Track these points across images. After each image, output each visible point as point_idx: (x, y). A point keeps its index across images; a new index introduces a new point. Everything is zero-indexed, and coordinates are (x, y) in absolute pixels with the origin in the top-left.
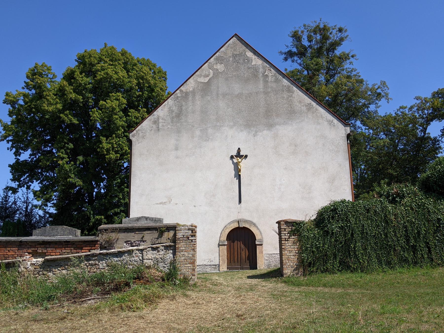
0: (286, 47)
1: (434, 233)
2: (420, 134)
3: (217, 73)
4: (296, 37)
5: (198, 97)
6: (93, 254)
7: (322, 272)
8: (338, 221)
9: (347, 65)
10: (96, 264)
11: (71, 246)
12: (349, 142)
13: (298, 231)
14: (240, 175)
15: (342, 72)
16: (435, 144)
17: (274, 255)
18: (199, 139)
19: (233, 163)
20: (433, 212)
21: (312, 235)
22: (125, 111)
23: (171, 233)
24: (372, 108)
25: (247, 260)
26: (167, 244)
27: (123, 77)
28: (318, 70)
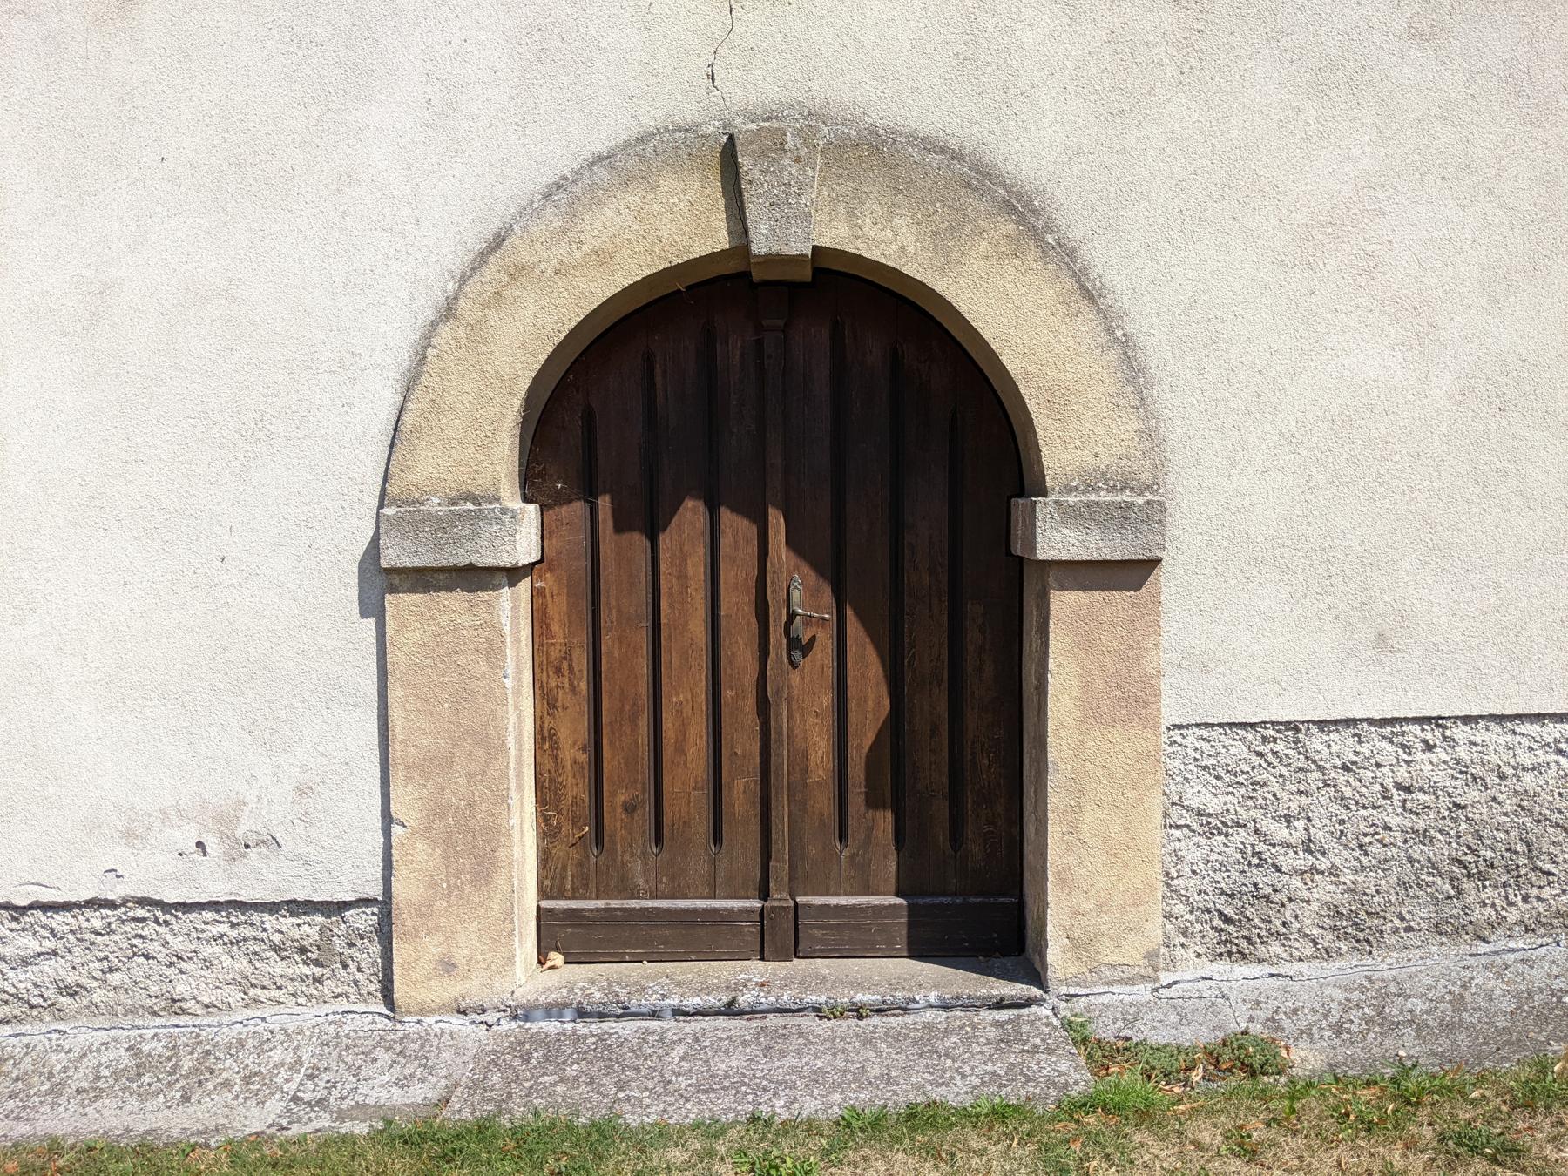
17: (1343, 745)
25: (873, 802)
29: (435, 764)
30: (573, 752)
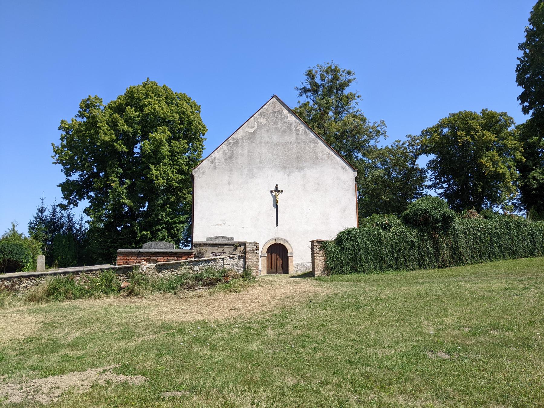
0: (301, 84)
1: (409, 250)
2: (409, 164)
3: (260, 126)
4: (311, 75)
5: (246, 143)
6: (190, 261)
7: (339, 274)
8: (350, 241)
9: (353, 104)
10: (192, 268)
11: (174, 255)
12: (356, 183)
13: (325, 247)
14: (277, 205)
15: (349, 110)
16: (422, 174)
18: (247, 177)
19: (272, 195)
20: (409, 237)
21: (334, 250)
22: (169, 141)
23: (242, 248)
24: (372, 142)
26: (240, 255)
27: (168, 112)
28: (329, 108)
29: (263, 264)
30: (268, 265)
